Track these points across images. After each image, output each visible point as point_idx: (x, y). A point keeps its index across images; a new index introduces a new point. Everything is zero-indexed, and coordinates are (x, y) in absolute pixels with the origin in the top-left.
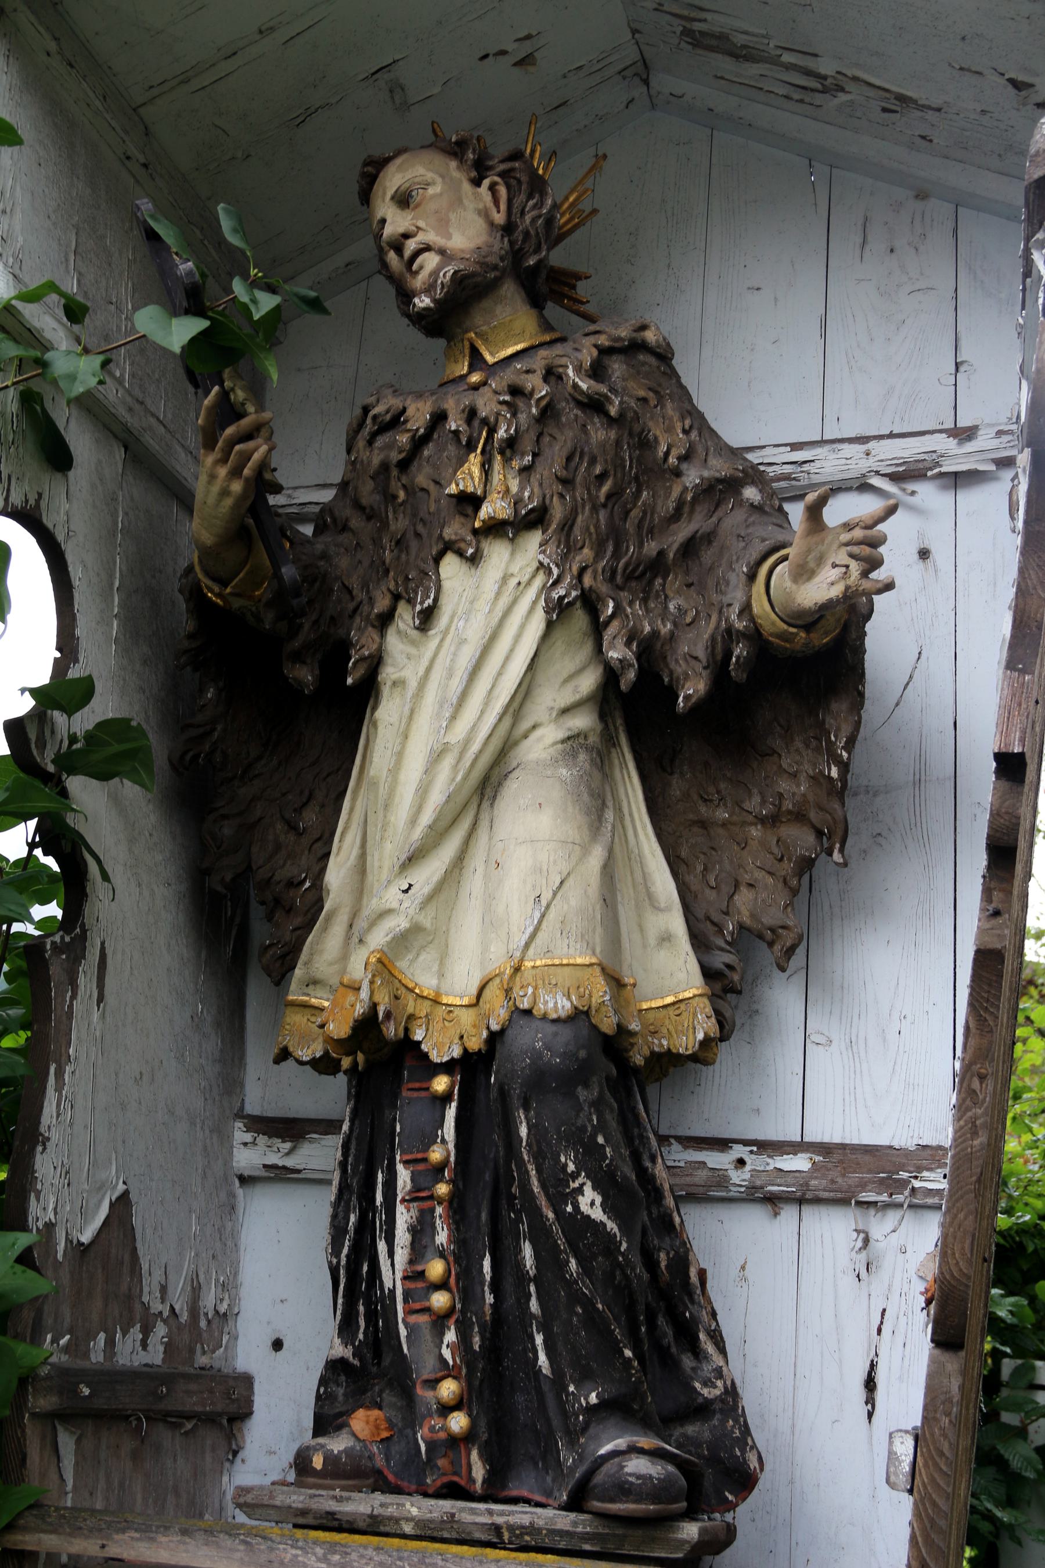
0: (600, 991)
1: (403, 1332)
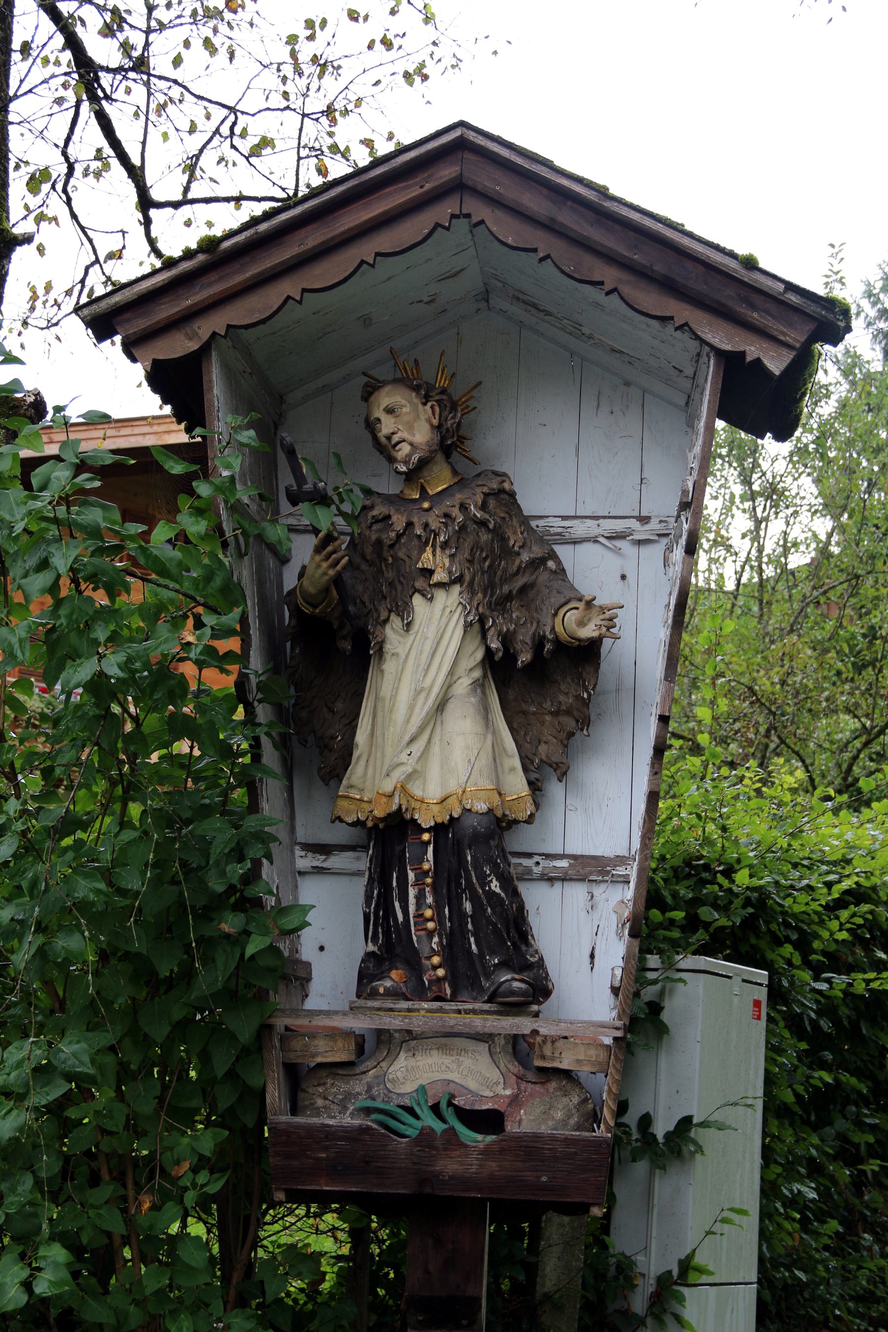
0: (496, 800)
1: (415, 938)
